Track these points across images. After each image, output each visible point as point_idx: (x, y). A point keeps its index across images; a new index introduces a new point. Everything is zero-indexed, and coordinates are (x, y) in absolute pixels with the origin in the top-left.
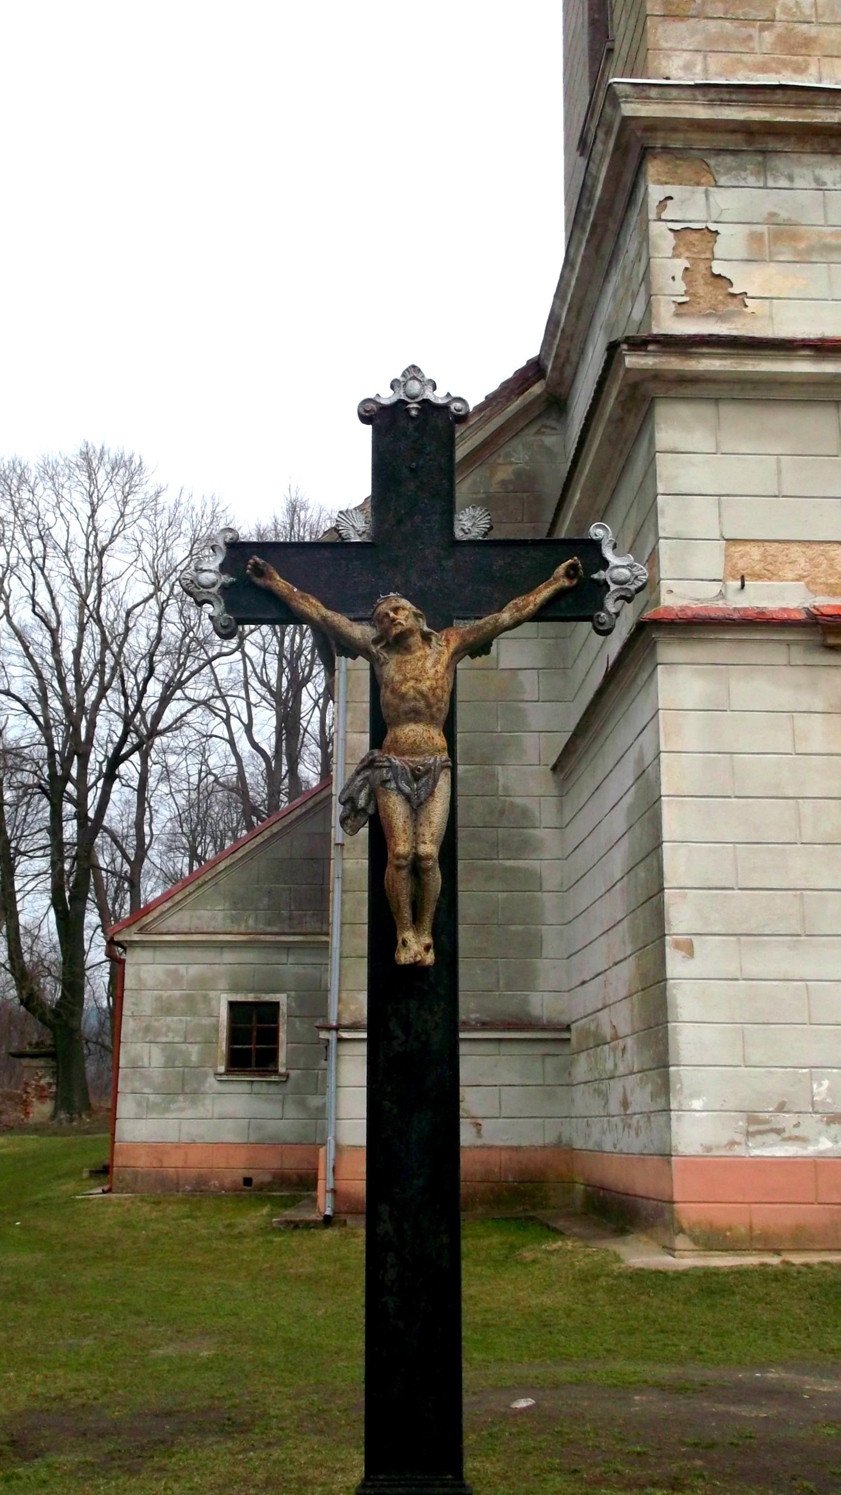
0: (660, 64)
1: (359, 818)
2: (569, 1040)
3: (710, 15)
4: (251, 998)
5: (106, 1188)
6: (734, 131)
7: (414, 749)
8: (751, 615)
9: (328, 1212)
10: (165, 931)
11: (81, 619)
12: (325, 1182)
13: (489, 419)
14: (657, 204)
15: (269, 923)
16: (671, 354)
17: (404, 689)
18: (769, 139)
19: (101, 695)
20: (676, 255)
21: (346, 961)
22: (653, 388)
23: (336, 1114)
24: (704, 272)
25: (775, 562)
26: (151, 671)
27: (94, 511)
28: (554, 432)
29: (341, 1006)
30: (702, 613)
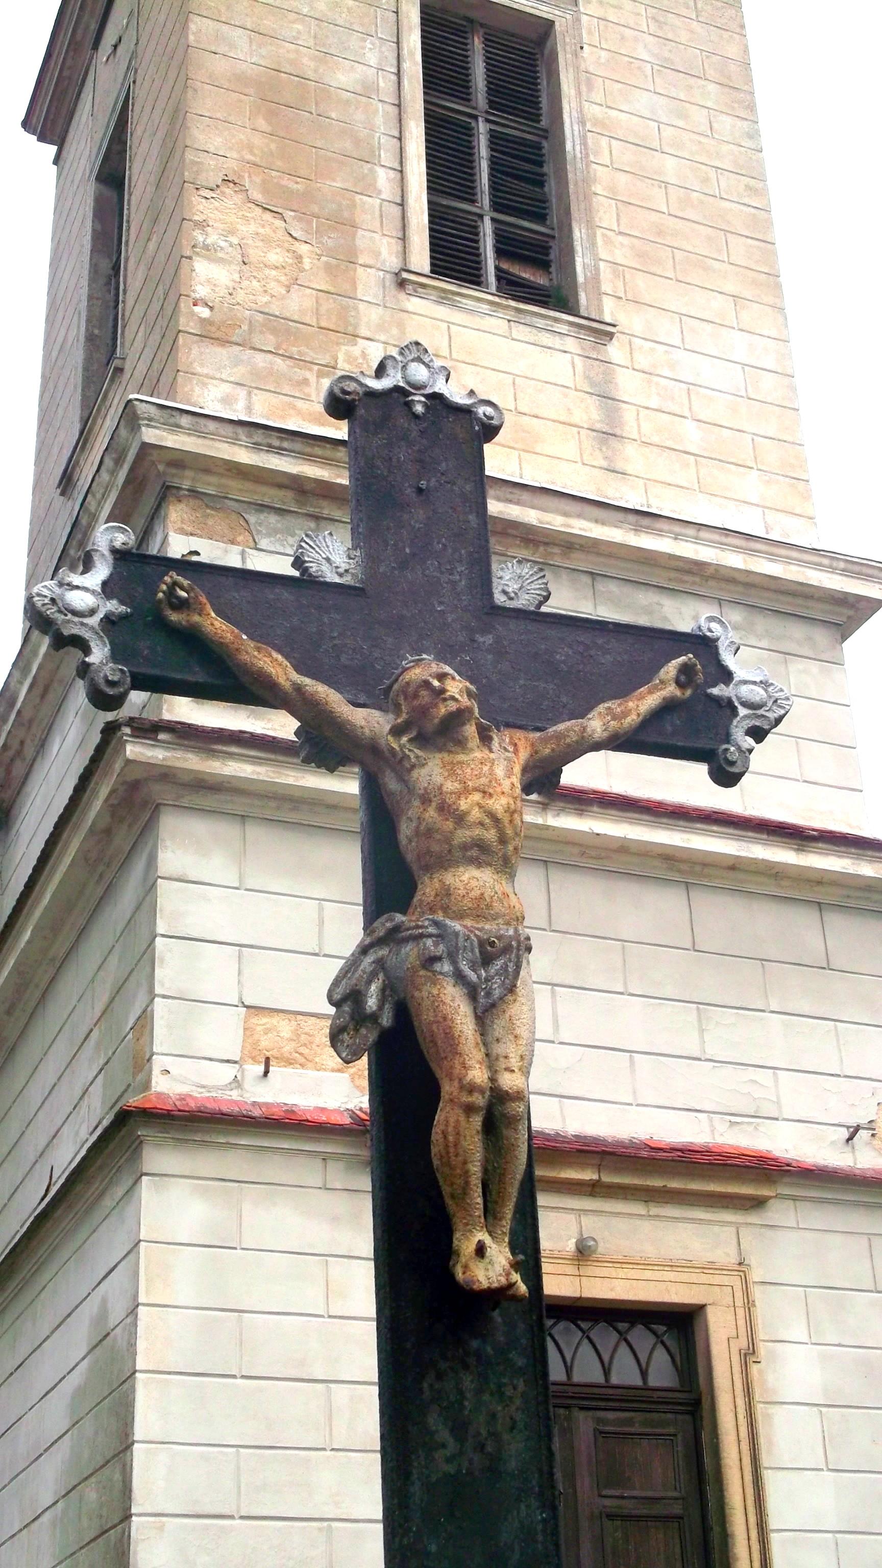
0: (192, 390)
1: (363, 1031)
3: (258, 346)
6: (280, 486)
8: (278, 1113)
16: (187, 748)
17: (464, 805)
18: (324, 503)
22: (158, 791)
25: (311, 1043)
30: (211, 1106)
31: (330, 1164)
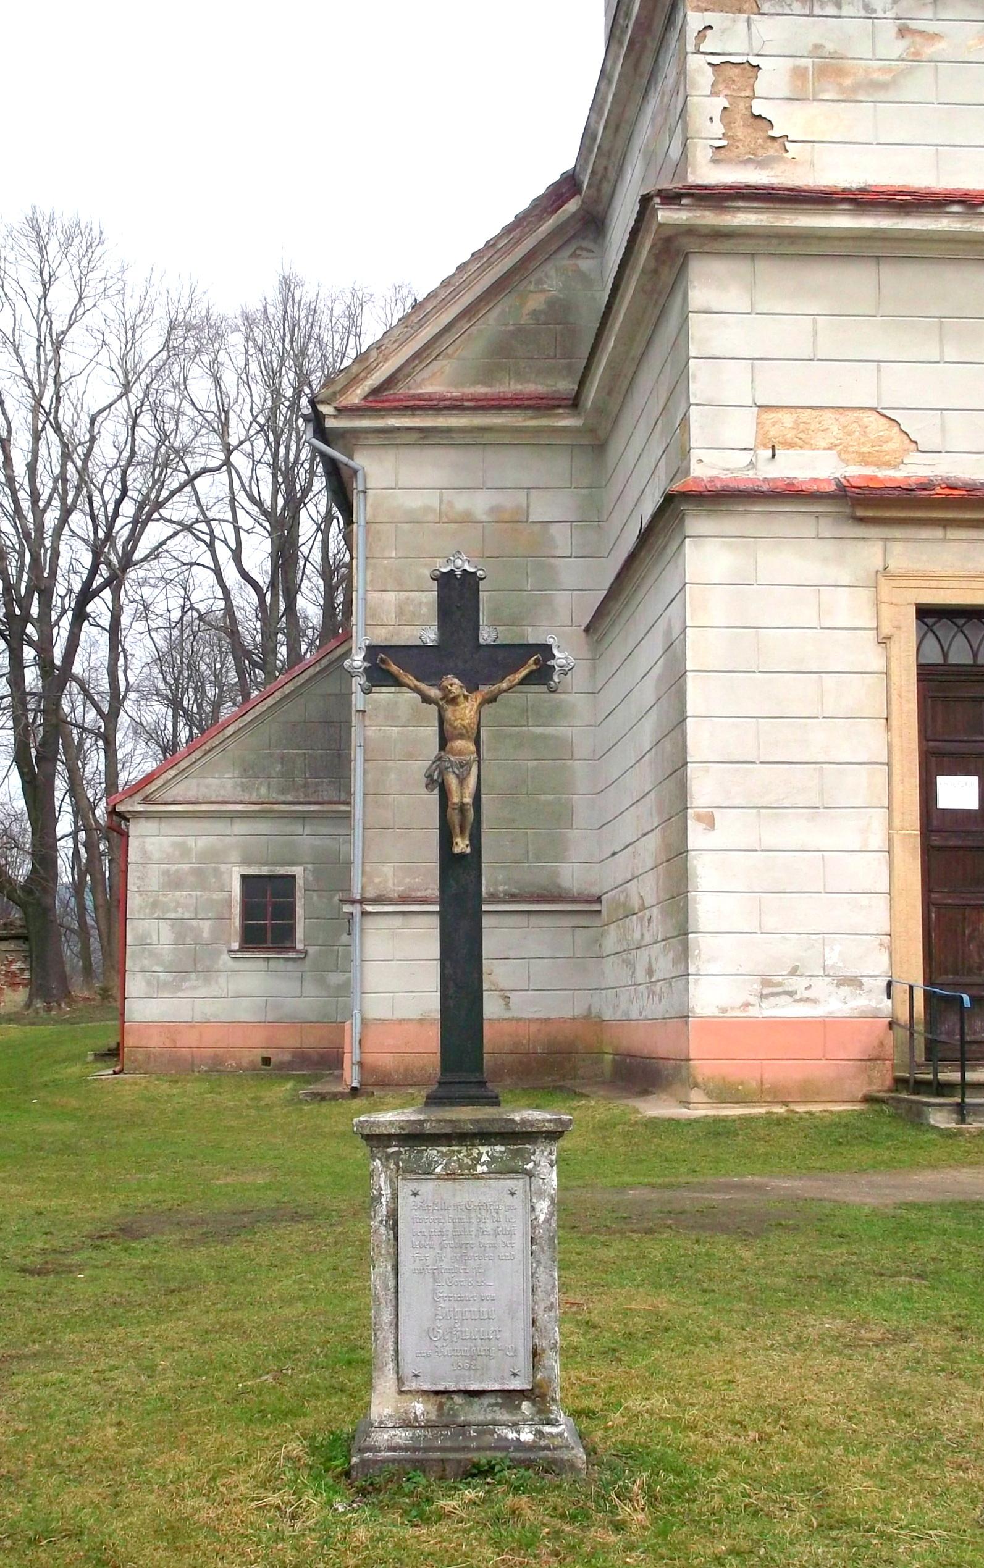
2: (599, 912)
4: (265, 871)
5: (117, 1069)
7: (460, 753)
8: (780, 487)
9: (355, 1084)
10: (170, 800)
11: (35, 426)
12: (351, 1056)
13: (519, 241)
14: (696, 34)
15: (283, 792)
16: (706, 207)
19: (63, 520)
20: (714, 94)
21: (369, 833)
23: (361, 986)
24: (744, 111)
26: (124, 491)
27: (46, 291)
28: (591, 255)
29: (365, 880)
30: (733, 485)
31: (822, 521)
